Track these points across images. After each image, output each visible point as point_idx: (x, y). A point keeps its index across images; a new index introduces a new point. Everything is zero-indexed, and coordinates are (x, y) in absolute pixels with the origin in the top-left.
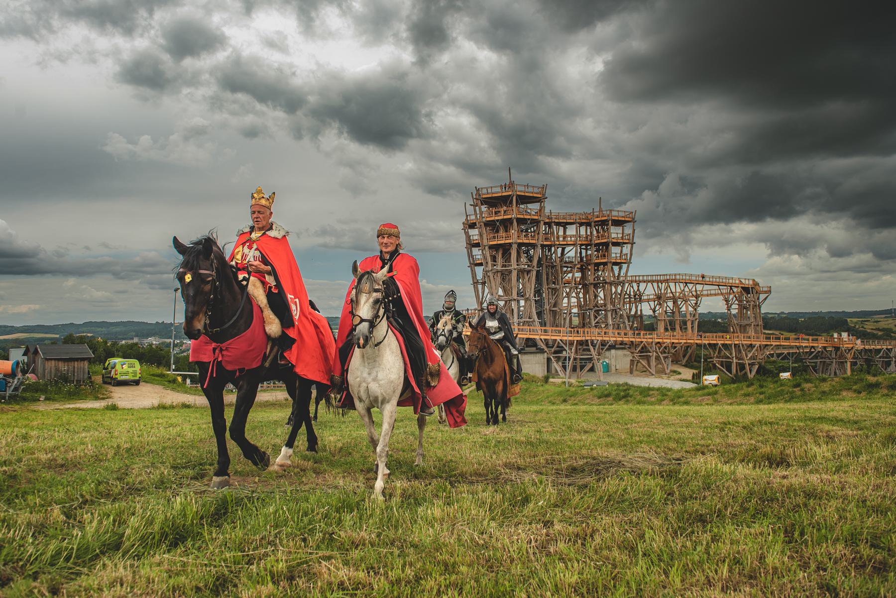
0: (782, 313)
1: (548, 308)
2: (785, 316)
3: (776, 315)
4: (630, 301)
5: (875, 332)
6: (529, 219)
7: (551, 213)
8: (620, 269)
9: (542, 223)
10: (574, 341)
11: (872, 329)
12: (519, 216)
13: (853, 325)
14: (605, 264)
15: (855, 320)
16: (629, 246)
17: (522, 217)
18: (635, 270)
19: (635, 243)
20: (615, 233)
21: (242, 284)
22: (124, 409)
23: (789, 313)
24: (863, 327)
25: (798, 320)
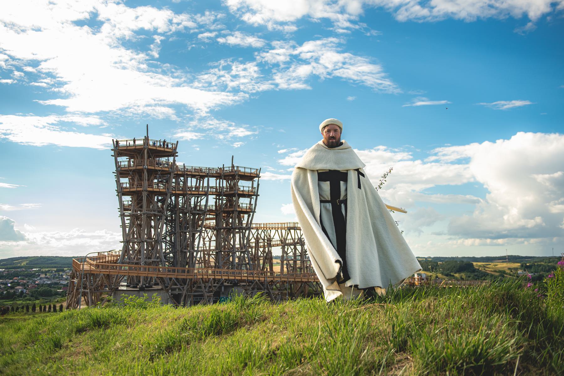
0: (430, 258)
1: (179, 249)
2: (430, 259)
3: (424, 259)
4: (264, 245)
5: (493, 273)
6: (159, 170)
7: (184, 166)
8: (249, 216)
9: (172, 175)
10: (187, 279)
11: (491, 271)
12: (150, 167)
13: (477, 268)
14: (233, 212)
15: (479, 264)
16: (255, 197)
17: (153, 168)
18: (259, 218)
19: (259, 195)
20: (244, 185)
21: (218, 42)
22: (19, 59)
23: (434, 258)
24: (485, 269)
25: (438, 263)
